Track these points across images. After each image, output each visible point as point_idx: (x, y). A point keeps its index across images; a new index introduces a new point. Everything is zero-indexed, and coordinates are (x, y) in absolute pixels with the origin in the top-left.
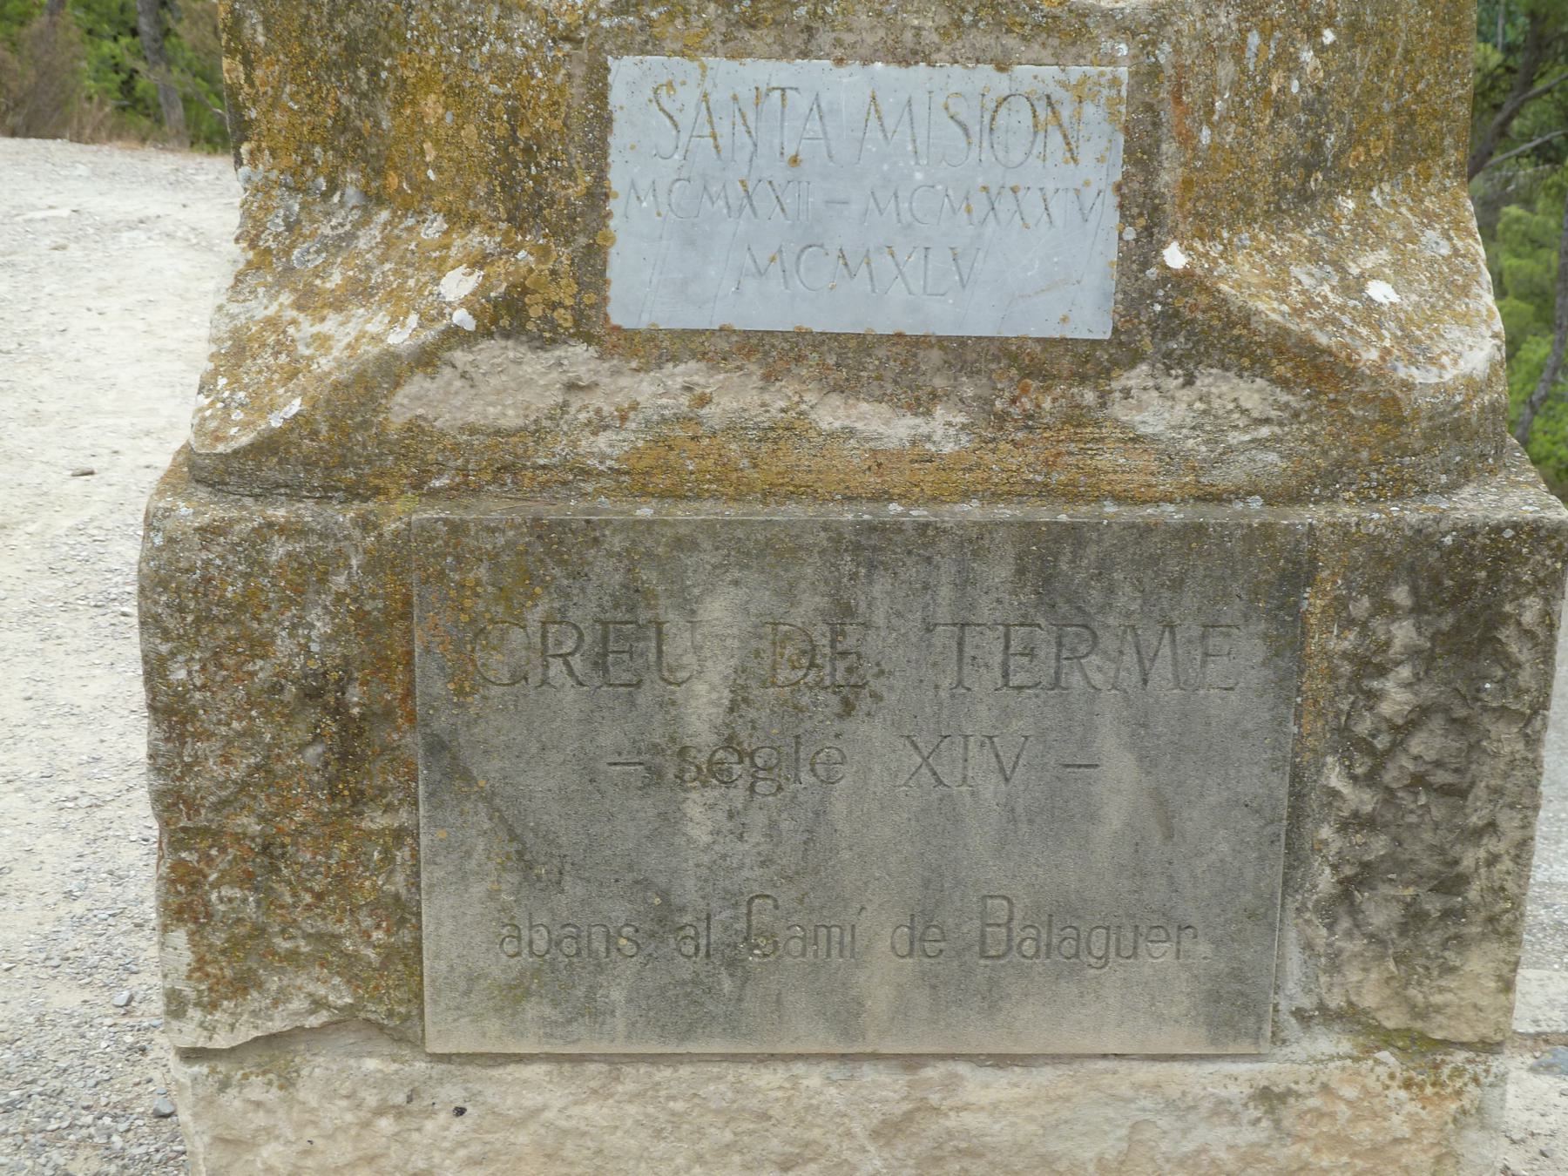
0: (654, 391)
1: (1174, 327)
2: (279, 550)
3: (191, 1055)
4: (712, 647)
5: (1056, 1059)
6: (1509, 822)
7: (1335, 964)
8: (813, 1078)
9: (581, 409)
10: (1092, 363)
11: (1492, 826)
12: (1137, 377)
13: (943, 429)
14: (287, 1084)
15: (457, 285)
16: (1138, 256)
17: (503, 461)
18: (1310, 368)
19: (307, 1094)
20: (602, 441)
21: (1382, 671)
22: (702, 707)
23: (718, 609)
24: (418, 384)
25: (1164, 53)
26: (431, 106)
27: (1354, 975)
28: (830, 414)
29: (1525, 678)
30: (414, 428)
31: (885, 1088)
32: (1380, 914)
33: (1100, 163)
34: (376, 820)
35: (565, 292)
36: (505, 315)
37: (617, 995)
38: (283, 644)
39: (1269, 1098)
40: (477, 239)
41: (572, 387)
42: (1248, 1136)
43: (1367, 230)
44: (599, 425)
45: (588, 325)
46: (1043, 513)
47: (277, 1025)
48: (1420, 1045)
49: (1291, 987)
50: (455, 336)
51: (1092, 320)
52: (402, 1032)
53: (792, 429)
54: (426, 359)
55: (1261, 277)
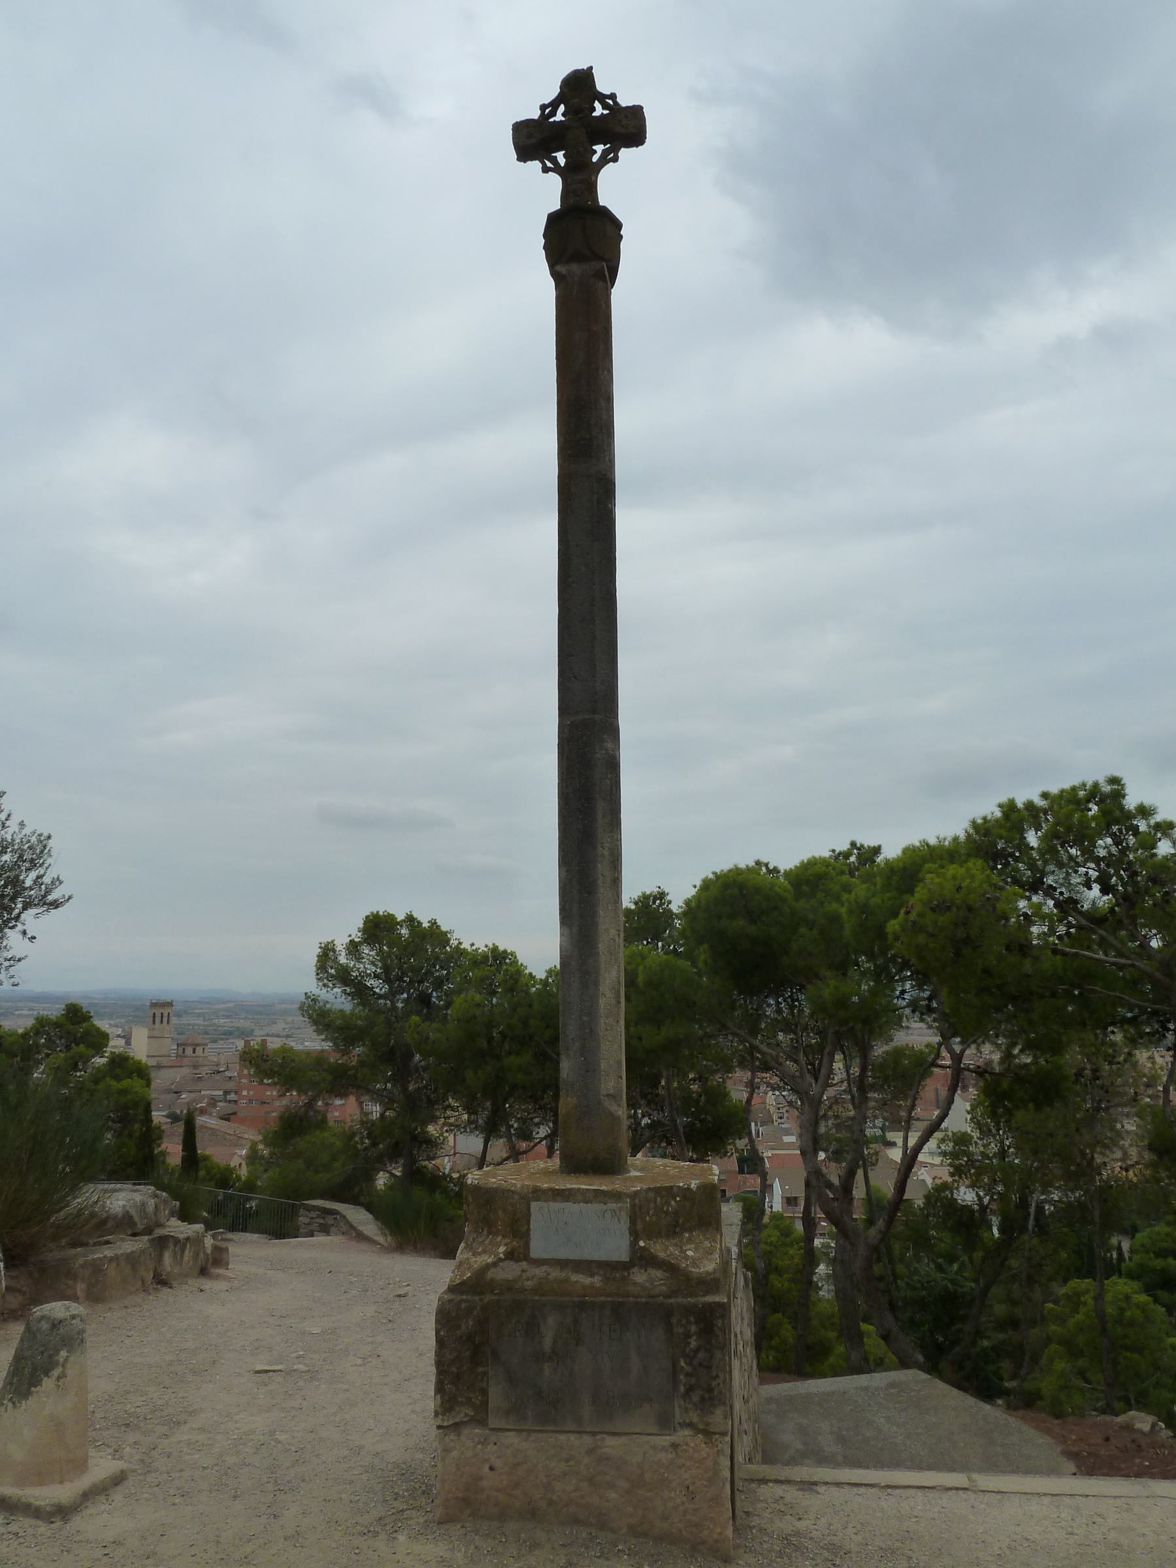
0: (539, 1272)
1: (641, 1259)
2: (463, 1306)
3: (439, 1427)
4: (550, 1326)
5: (626, 1434)
6: (721, 1375)
7: (687, 1411)
8: (572, 1437)
9: (525, 1276)
10: (626, 1266)
11: (717, 1376)
12: (635, 1270)
13: (597, 1281)
14: (459, 1435)
15: (502, 1249)
16: (634, 1243)
17: (509, 1286)
18: (670, 1268)
19: (463, 1438)
20: (529, 1283)
21: (690, 1337)
22: (547, 1343)
23: (551, 1320)
24: (493, 1270)
25: (637, 1201)
26: (500, 1213)
27: (691, 1414)
28: (574, 1278)
29: (721, 1339)
30: (492, 1280)
31: (587, 1439)
32: (695, 1397)
33: (624, 1224)
34: (481, 1369)
35: (521, 1250)
36: (510, 1255)
37: (530, 1414)
38: (463, 1326)
39: (674, 1446)
40: (507, 1240)
41: (523, 1271)
42: (670, 1456)
43: (690, 1241)
44: (528, 1279)
45: (526, 1257)
46: (616, 1299)
47: (457, 1420)
48: (708, 1434)
49: (677, 1416)
50: (500, 1260)
51: (623, 1255)
52: (482, 1422)
53: (567, 1280)
54: (495, 1264)
55: (662, 1249)
